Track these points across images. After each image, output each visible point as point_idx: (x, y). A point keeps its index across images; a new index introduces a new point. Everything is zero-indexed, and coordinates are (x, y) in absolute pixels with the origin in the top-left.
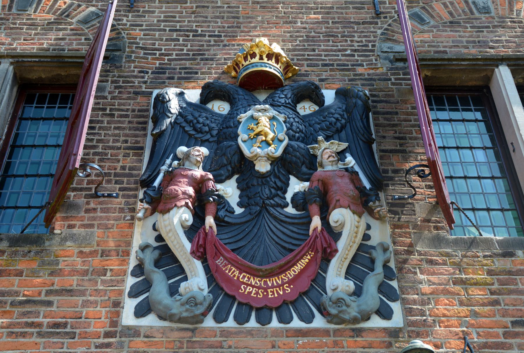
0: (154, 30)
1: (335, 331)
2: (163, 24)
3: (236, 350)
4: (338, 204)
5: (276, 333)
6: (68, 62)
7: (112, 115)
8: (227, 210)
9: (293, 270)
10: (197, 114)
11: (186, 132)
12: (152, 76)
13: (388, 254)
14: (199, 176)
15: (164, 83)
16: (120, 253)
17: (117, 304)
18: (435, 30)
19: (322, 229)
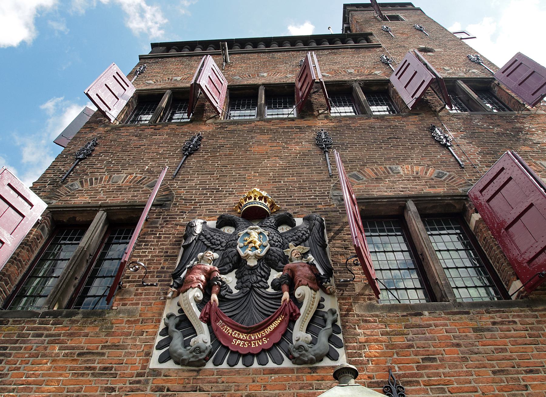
0: (192, 189)
1: (298, 369)
3: (227, 384)
4: (300, 283)
5: (256, 372)
6: (137, 208)
8: (227, 291)
9: (269, 328)
10: (212, 234)
11: (205, 244)
13: (335, 316)
14: (209, 269)
16: (154, 321)
17: (148, 354)
18: (366, 183)
19: (290, 301)
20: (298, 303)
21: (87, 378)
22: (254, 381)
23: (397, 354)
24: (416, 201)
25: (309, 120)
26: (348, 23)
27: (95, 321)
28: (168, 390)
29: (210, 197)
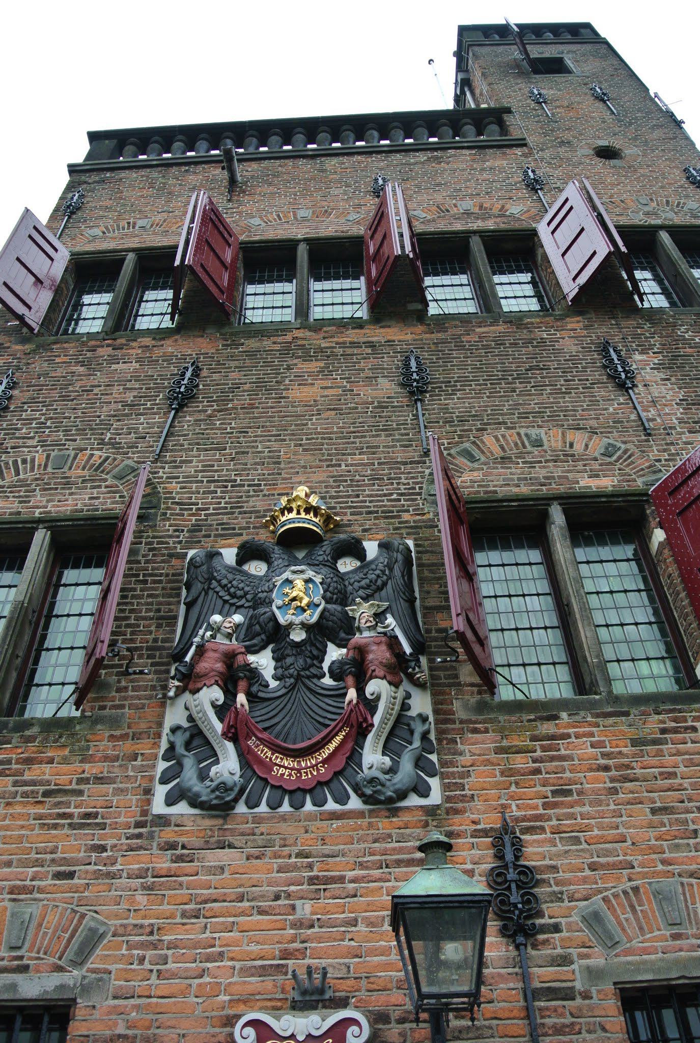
0: (191, 482)
2: (200, 474)
3: (269, 837)
4: (374, 674)
5: (311, 817)
7: (145, 582)
10: (230, 576)
12: (187, 535)
15: (200, 542)
16: (152, 736)
17: (148, 792)
18: (485, 467)
19: (358, 702)
20: (371, 705)
21: (63, 832)
22: (307, 832)
23: (517, 784)
24: (565, 504)
25: (389, 327)
26: (467, 71)
27: (60, 737)
28: (184, 847)
29: (221, 498)
